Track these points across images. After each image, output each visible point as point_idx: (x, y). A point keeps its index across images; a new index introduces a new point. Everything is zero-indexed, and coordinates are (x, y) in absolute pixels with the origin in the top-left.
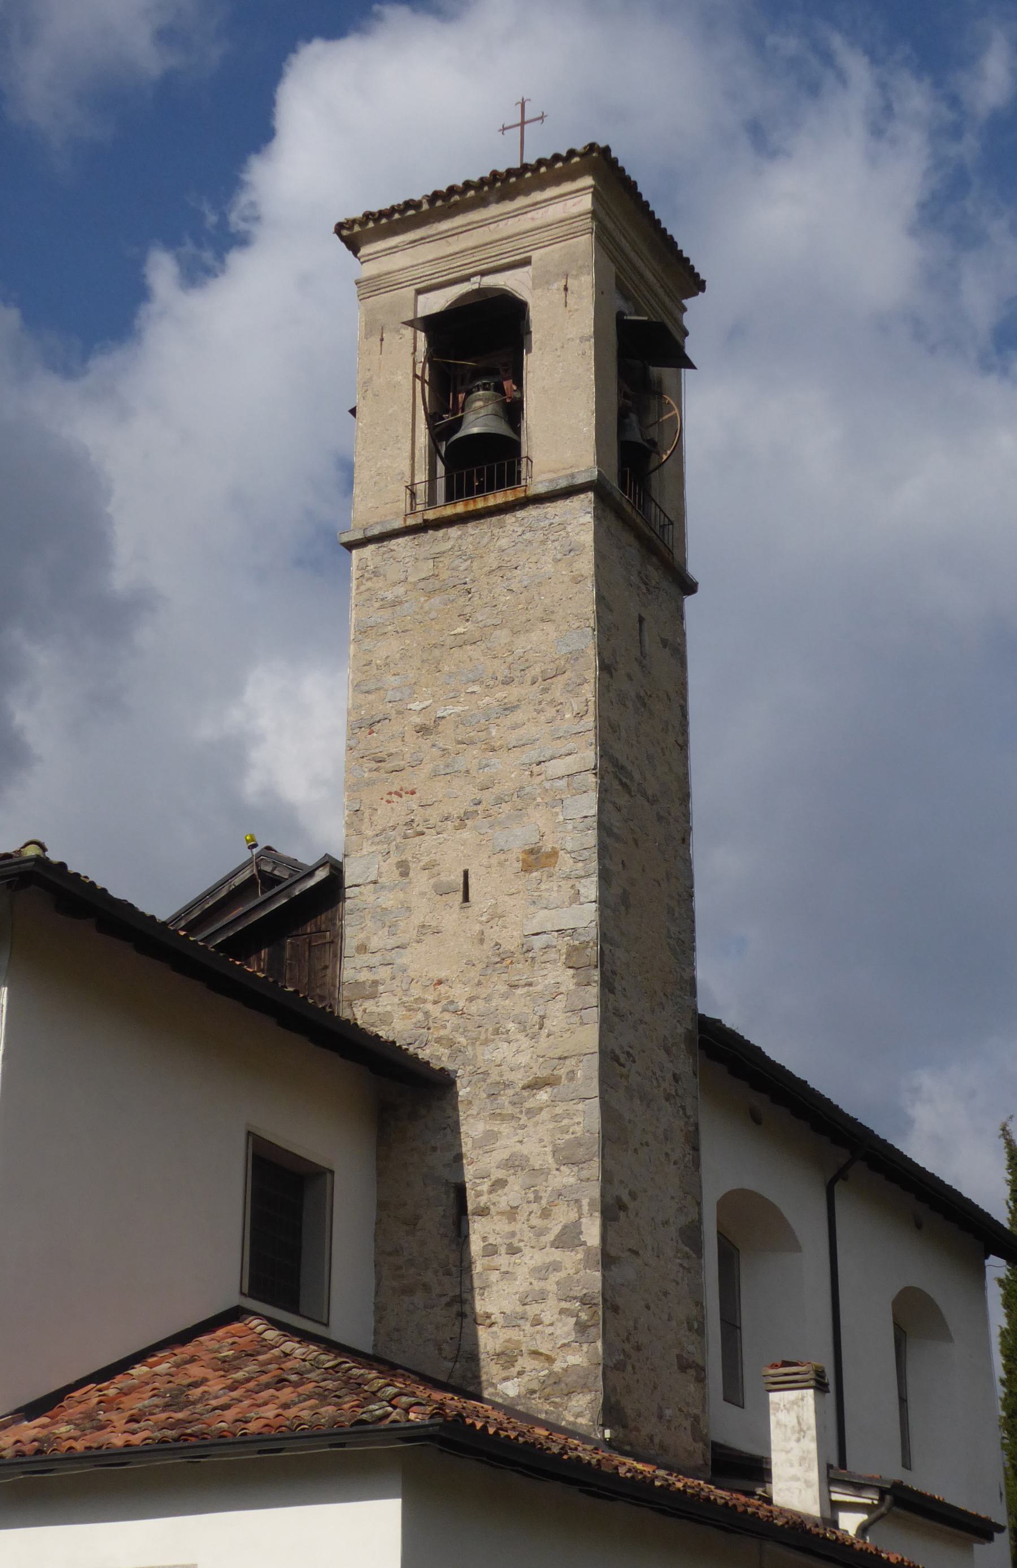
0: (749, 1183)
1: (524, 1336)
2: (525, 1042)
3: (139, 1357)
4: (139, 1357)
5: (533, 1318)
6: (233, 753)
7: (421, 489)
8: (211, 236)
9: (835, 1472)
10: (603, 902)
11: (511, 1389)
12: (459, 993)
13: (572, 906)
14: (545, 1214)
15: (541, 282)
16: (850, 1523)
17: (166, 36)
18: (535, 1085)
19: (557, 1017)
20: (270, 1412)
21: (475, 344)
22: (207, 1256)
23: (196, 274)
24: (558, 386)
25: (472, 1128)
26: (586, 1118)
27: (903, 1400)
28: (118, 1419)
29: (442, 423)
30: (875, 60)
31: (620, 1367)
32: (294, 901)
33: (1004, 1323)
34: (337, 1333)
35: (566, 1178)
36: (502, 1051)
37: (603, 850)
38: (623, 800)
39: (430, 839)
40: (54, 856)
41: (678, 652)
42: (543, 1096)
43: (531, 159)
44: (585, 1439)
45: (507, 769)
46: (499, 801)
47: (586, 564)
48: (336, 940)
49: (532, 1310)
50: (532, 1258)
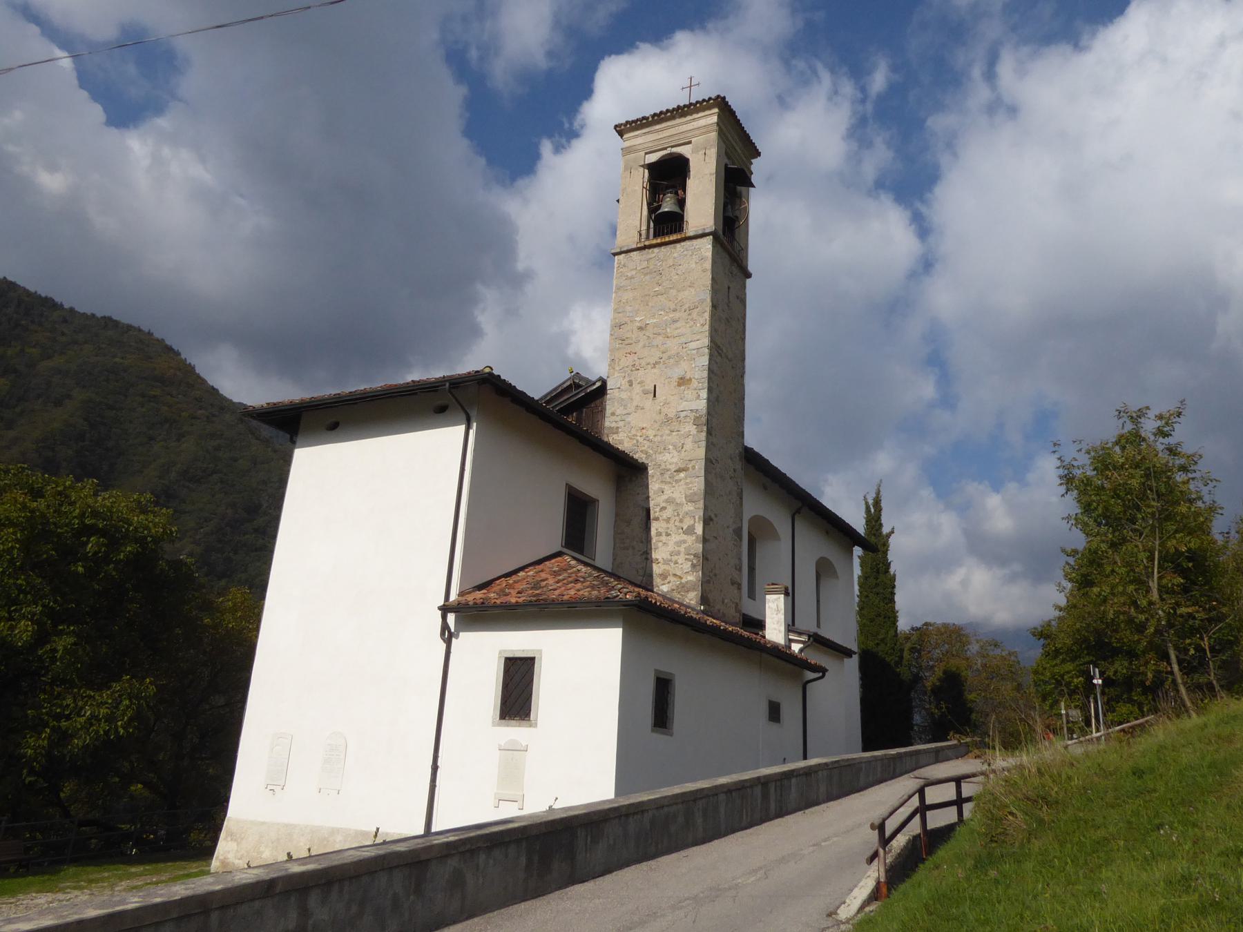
0: (761, 513)
1: (671, 568)
2: (675, 453)
3: (522, 569)
4: (522, 569)
5: (675, 562)
6: (564, 338)
7: (644, 233)
8: (565, 131)
9: (791, 627)
10: (709, 399)
11: (665, 588)
12: (651, 433)
13: (698, 401)
14: (681, 521)
15: (695, 151)
16: (796, 648)
17: (550, 54)
18: (679, 471)
19: (689, 444)
20: (572, 592)
21: (668, 174)
22: (552, 534)
23: (558, 149)
24: (700, 194)
25: (654, 486)
26: (698, 484)
27: (818, 601)
28: (514, 592)
29: (653, 206)
30: (832, 71)
31: (708, 582)
32: (587, 394)
33: (860, 573)
34: (598, 563)
35: (690, 507)
36: (667, 457)
37: (710, 379)
38: (719, 359)
39: (641, 372)
40: (496, 372)
41: (743, 302)
42: (682, 475)
43: (693, 101)
44: (693, 609)
45: (673, 345)
46: (669, 358)
47: (708, 265)
48: (603, 410)
49: (674, 558)
50: (675, 538)
